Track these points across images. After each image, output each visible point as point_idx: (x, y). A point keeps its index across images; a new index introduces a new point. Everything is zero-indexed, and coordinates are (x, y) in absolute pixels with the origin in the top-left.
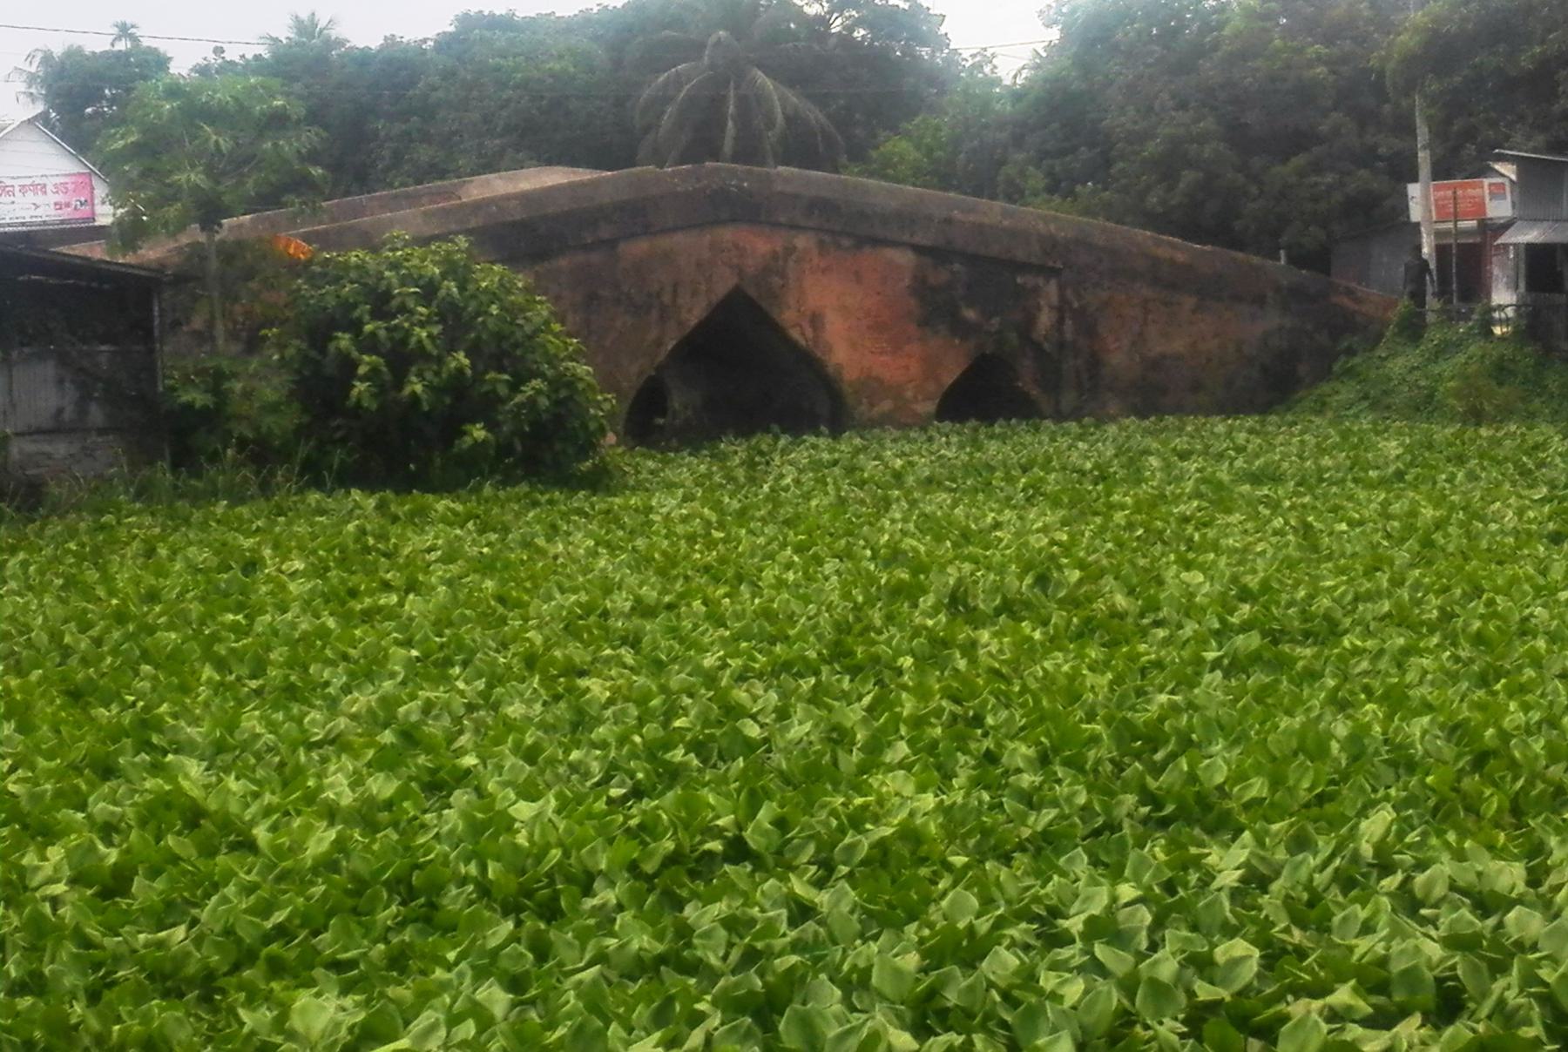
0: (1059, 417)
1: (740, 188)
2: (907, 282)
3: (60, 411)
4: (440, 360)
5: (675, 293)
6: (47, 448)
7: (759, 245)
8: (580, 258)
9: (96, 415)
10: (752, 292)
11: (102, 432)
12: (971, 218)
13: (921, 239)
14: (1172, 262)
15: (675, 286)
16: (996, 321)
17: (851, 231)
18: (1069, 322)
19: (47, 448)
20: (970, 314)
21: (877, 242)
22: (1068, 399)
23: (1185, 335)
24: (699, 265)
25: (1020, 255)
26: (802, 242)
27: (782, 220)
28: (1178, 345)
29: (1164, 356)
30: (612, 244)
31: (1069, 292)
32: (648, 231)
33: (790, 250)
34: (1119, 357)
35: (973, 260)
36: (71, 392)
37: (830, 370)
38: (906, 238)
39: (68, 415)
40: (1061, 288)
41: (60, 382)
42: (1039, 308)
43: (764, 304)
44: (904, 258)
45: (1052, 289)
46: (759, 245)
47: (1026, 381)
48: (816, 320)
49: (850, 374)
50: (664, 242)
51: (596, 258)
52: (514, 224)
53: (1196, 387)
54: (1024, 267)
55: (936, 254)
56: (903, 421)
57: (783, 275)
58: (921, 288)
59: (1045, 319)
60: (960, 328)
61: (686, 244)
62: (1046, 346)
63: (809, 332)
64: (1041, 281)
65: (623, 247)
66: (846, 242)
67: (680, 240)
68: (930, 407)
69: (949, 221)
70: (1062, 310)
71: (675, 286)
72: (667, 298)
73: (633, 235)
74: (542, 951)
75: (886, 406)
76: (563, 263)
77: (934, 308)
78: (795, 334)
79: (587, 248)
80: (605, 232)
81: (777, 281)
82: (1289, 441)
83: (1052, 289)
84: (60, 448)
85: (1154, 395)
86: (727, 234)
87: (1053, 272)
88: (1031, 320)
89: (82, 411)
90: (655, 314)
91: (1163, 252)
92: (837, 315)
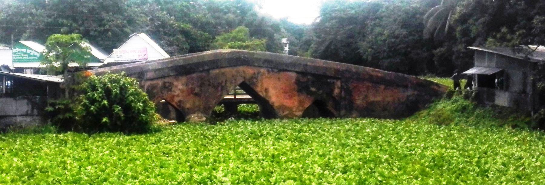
0: (341, 117)
1: (244, 57)
2: (294, 80)
3: (27, 111)
4: (100, 102)
5: (226, 83)
6: (25, 119)
7: (250, 71)
8: (200, 74)
9: (35, 111)
10: (248, 83)
11: (37, 116)
12: (313, 64)
13: (297, 70)
14: (377, 76)
15: (226, 81)
16: (321, 91)
17: (277, 67)
18: (343, 92)
19: (25, 119)
20: (313, 89)
21: (286, 70)
22: (343, 112)
23: (378, 97)
24: (233, 76)
25: (328, 74)
26: (262, 70)
27: (257, 65)
28: (379, 99)
29: (373, 101)
30: (208, 71)
31: (343, 84)
32: (217, 67)
33: (259, 73)
34: (359, 101)
35: (313, 75)
36: (30, 106)
37: (270, 103)
38: (293, 69)
39: (29, 112)
40: (342, 82)
41: (28, 104)
42: (335, 88)
43: (251, 86)
44: (293, 75)
45: (339, 83)
46: (250, 71)
47: (330, 107)
48: (266, 90)
49: (276, 105)
50: (223, 70)
51: (204, 74)
52: (180, 66)
53: (385, 110)
54: (330, 77)
55: (303, 74)
56: (290, 117)
57: (256, 79)
58: (298, 82)
59: (336, 91)
60: (310, 93)
61: (228, 70)
62: (337, 98)
63: (265, 94)
64: (335, 81)
65: (211, 71)
66: (276, 70)
67: (227, 70)
68: (299, 113)
69: (306, 65)
70: (342, 88)
71: (226, 81)
72: (223, 84)
73: (214, 68)
74: (335, 159)
75: (287, 113)
76: (195, 75)
77: (301, 87)
78: (260, 94)
79: (201, 72)
80: (206, 68)
81: (255, 80)
82: (412, 125)
83: (339, 83)
84: (28, 119)
85: (370, 111)
86: (241, 68)
87: (338, 79)
88: (332, 91)
89: (32, 111)
90: (220, 88)
91: (374, 74)
92: (273, 90)
